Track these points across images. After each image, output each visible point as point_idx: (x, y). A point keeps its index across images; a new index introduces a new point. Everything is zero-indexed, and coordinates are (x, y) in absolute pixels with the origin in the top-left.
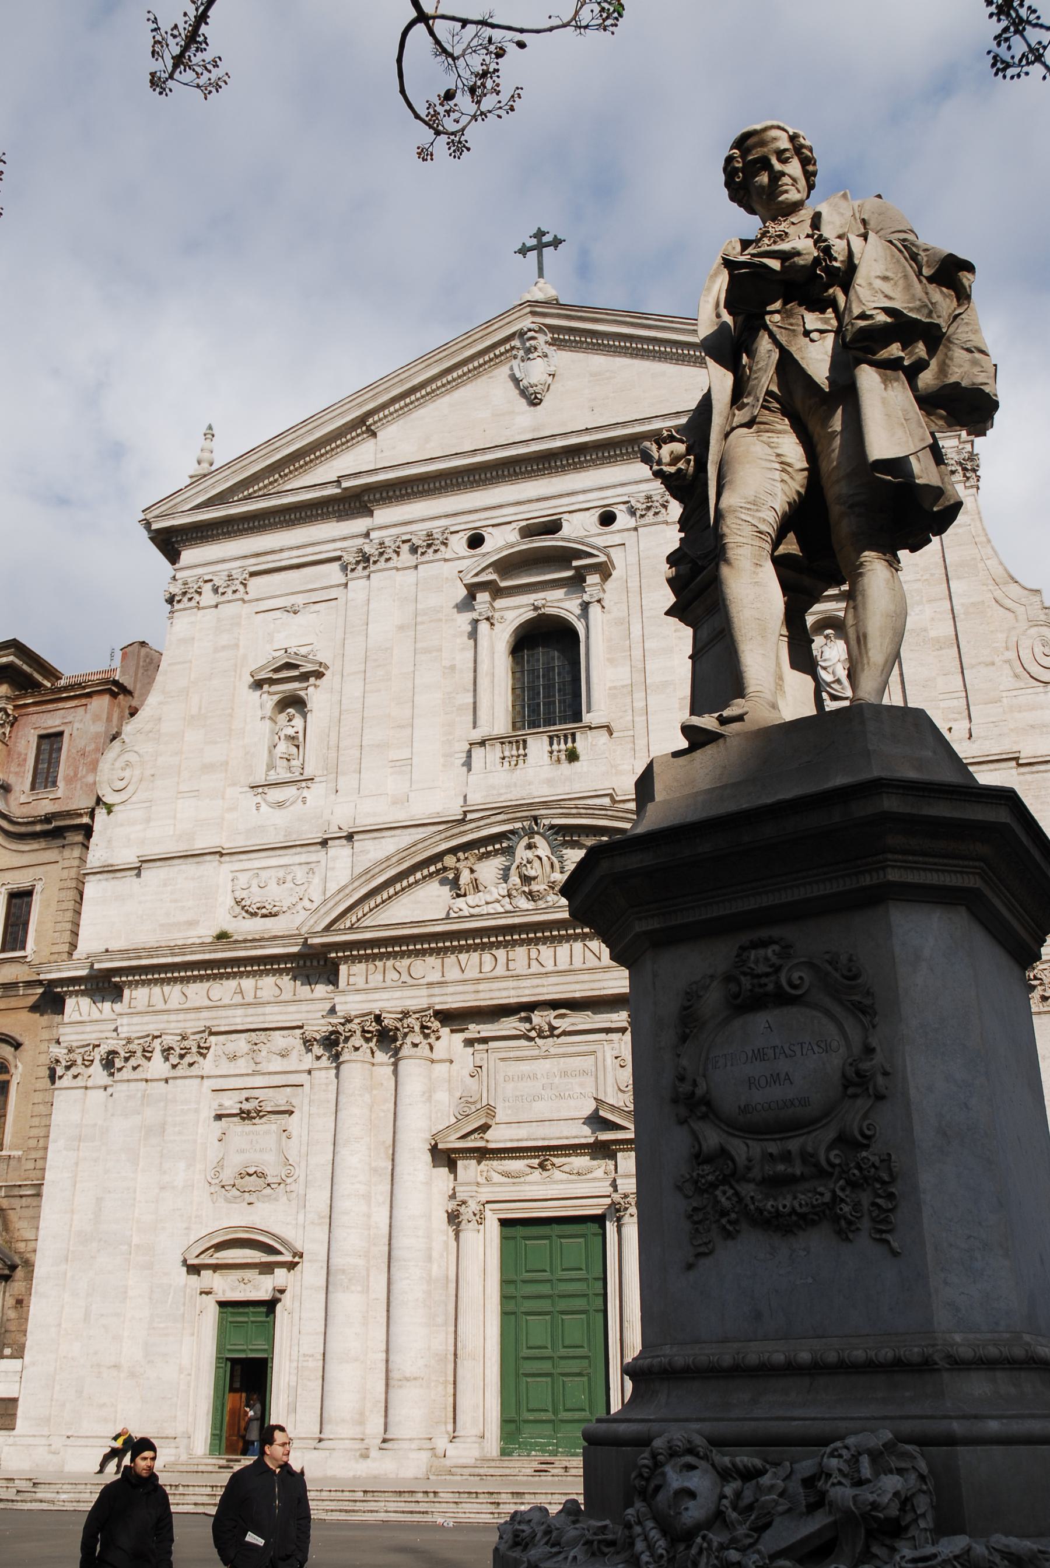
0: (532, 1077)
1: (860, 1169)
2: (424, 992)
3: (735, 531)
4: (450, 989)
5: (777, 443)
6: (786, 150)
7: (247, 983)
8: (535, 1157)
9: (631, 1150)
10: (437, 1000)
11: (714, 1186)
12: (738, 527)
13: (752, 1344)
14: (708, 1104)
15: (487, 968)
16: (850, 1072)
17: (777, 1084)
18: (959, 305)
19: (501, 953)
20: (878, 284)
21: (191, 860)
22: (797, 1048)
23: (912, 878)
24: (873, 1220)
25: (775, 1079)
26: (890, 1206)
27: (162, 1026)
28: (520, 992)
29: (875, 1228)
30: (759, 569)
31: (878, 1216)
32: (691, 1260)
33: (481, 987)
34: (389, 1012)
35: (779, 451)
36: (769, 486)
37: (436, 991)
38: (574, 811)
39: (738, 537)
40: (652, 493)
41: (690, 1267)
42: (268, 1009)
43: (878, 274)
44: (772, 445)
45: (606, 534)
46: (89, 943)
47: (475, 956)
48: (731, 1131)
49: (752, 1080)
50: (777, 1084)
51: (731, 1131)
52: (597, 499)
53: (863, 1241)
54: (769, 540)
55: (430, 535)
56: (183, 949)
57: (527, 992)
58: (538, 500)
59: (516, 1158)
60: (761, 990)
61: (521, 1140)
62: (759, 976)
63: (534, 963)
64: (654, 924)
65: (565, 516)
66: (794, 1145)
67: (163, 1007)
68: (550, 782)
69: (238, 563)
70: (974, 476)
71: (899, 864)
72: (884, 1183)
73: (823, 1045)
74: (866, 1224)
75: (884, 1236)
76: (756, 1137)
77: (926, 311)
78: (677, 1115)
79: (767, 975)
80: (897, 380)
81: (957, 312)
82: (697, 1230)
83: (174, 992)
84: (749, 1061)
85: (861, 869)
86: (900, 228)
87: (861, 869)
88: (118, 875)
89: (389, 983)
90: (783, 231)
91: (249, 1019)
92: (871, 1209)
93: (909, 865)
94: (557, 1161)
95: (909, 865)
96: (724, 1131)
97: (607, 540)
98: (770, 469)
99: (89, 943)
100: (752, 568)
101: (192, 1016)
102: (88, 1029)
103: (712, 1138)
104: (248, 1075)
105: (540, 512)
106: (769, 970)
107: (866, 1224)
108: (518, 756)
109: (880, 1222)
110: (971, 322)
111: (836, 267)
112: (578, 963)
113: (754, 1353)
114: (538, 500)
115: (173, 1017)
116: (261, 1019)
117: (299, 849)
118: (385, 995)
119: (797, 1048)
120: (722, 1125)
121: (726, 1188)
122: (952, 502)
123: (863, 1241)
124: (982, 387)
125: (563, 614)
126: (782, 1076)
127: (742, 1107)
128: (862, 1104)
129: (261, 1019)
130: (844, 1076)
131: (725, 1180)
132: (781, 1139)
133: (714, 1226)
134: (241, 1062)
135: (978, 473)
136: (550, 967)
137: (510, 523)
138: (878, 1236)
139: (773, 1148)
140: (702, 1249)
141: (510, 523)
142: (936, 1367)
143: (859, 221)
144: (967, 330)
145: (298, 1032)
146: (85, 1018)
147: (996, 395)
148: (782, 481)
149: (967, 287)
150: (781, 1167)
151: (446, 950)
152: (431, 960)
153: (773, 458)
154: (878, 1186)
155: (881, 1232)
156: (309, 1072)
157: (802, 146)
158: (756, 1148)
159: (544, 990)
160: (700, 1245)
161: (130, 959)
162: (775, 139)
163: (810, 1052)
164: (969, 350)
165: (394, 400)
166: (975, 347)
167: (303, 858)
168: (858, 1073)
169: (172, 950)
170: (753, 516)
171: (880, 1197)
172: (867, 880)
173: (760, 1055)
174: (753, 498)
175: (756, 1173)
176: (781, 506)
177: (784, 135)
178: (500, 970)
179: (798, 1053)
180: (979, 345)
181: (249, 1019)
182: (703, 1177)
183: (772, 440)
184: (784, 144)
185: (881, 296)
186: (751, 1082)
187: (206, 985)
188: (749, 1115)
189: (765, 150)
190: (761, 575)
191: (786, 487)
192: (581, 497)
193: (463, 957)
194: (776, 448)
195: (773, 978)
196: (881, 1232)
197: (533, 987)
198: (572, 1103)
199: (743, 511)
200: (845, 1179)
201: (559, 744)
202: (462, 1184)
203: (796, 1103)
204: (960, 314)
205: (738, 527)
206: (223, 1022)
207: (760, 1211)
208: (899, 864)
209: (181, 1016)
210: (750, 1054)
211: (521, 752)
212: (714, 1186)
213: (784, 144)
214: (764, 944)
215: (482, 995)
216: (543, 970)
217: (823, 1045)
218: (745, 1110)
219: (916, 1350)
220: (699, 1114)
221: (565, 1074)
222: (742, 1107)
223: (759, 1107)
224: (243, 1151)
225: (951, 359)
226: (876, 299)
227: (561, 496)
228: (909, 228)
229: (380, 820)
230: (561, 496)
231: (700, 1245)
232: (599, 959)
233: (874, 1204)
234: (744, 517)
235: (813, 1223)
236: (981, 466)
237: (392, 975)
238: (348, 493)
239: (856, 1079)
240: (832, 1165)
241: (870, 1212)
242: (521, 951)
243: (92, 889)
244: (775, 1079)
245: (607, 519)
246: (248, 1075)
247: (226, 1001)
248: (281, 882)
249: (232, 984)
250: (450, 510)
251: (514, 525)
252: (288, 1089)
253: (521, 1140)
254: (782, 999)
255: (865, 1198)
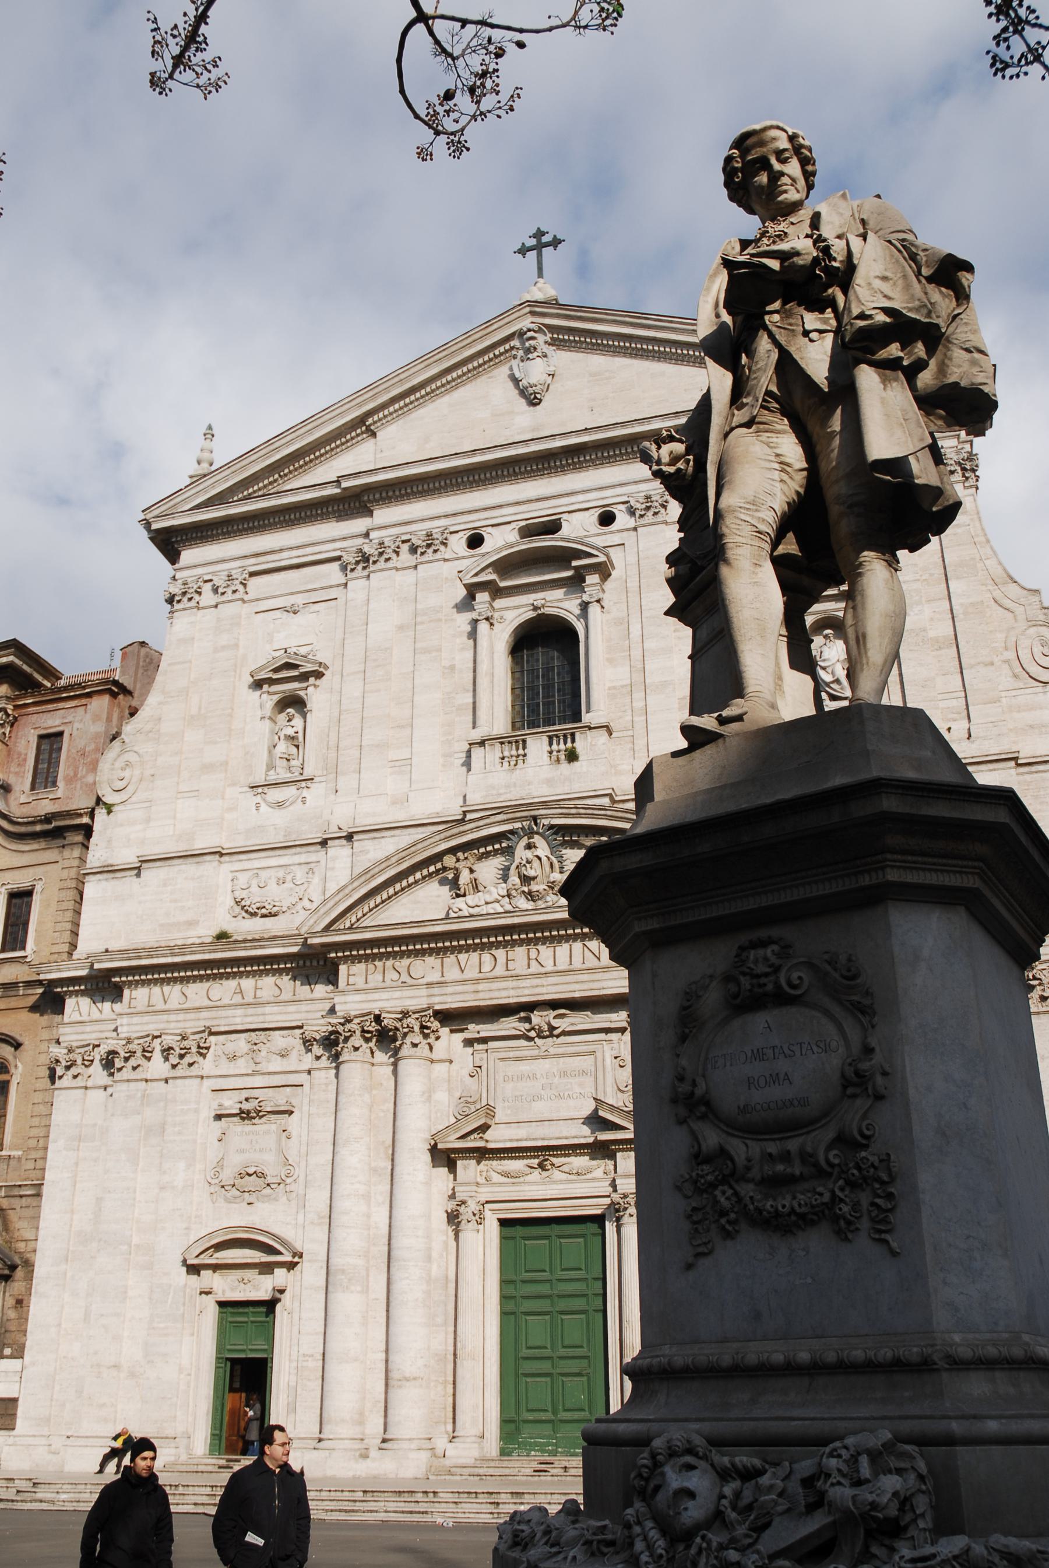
0: (532, 1077)
1: (859, 1169)
2: (424, 992)
3: (734, 531)
4: (450, 989)
5: (777, 443)
6: (785, 150)
7: (247, 983)
8: (535, 1157)
9: (630, 1150)
10: (436, 1000)
11: (713, 1186)
12: (738, 527)
13: (751, 1344)
14: (707, 1104)
15: (486, 968)
16: (850, 1072)
17: (777, 1084)
18: (958, 305)
19: (500, 953)
20: (878, 284)
21: (190, 860)
22: (796, 1048)
23: (911, 878)
24: (873, 1220)
25: (775, 1079)
26: (889, 1206)
27: (162, 1026)
28: (520, 992)
29: (874, 1228)
30: (758, 569)
31: (877, 1216)
32: (691, 1260)
33: (480, 987)
34: (389, 1012)
35: (778, 451)
36: (768, 486)
37: (436, 991)
38: (574, 811)
39: (737, 537)
40: (651, 493)
41: (689, 1267)
42: (268, 1009)
43: (878, 274)
44: (772, 445)
45: (605, 534)
46: (89, 943)
47: (474, 956)
48: (730, 1131)
49: (752, 1080)
50: (777, 1084)
51: (730, 1131)
52: (596, 499)
53: (863, 1241)
54: (768, 540)
55: (429, 535)
56: (183, 949)
57: (527, 992)
58: (538, 500)
59: (516, 1158)
60: (761, 990)
61: (521, 1140)
62: (758, 976)
63: (533, 963)
64: (653, 924)
65: (564, 516)
66: (793, 1145)
67: (163, 1007)
68: (549, 782)
69: (238, 563)
70: (973, 476)
71: (898, 864)
72: (883, 1183)
73: (822, 1045)
74: (865, 1224)
75: (883, 1236)
76: (755, 1137)
77: (925, 311)
78: (676, 1115)
79: (766, 975)
80: (896, 380)
81: (956, 312)
82: (696, 1230)
83: (174, 992)
84: (749, 1061)
85: (860, 869)
86: (899, 228)
87: (860, 869)
88: (118, 875)
89: (388, 983)
90: (783, 231)
91: (249, 1019)
92: (871, 1209)
93: (908, 865)
94: (556, 1161)
95: (908, 865)
96: (723, 1131)
97: (606, 540)
98: (770, 469)
99: (89, 943)
100: (752, 568)
101: (192, 1016)
102: (88, 1029)
103: (712, 1138)
104: (247, 1075)
105: (540, 512)
106: (768, 970)
107: (865, 1224)
108: (518, 756)
109: (879, 1222)
110: (971, 322)
111: (836, 267)
112: (577, 963)
113: (754, 1353)
114: (538, 500)
115: (173, 1017)
116: (261, 1019)
117: (298, 849)
118: (385, 995)
119: (796, 1048)
120: (722, 1125)
121: (726, 1188)
122: (951, 502)
123: (863, 1241)
124: (981, 387)
125: (563, 614)
126: (782, 1076)
127: (742, 1107)
128: (861, 1104)
129: (261, 1019)
130: (843, 1076)
131: (724, 1180)
132: (780, 1139)
133: (713, 1226)
134: (241, 1062)
135: (977, 473)
136: (549, 967)
137: (509, 523)
138: (877, 1236)
139: (772, 1148)
140: (701, 1249)
141: (509, 523)
142: (935, 1367)
143: (858, 221)
144: (966, 330)
145: (298, 1032)
146: (85, 1018)
147: (995, 395)
148: (782, 481)
149: (966, 287)
150: (780, 1167)
151: (445, 950)
152: (431, 960)
153: (773, 458)
154: (877, 1186)
155: (880, 1232)
156: (309, 1072)
157: (802, 146)
158: (756, 1148)
159: (544, 990)
160: (699, 1245)
161: (130, 959)
162: (774, 139)
163: (809, 1052)
164: (968, 350)
165: (393, 400)
166: (974, 347)
167: (303, 858)
168: (857, 1073)
169: (172, 950)
170: (753, 516)
171: (880, 1197)
172: (866, 880)
173: (759, 1055)
174: (752, 498)
175: (755, 1173)
176: (781, 506)
177: (784, 135)
178: (500, 970)
179: (798, 1053)
180: (978, 345)
181: (249, 1019)
182: (702, 1177)
183: (771, 440)
184: (784, 144)
185: (880, 296)
186: (750, 1082)
187: (206, 985)
188: (748, 1115)
189: (765, 150)
190: (760, 575)
191: (785, 487)
192: (581, 497)
193: (463, 957)
194: (775, 448)
195: (772, 978)
196: (880, 1232)
197: (533, 987)
198: (571, 1103)
199: (743, 511)
200: (844, 1179)
201: (558, 744)
202: (461, 1184)
203: (796, 1103)
204: (959, 314)
205: (738, 527)
206: (223, 1022)
207: (760, 1211)
208: (898, 864)
209: (181, 1016)
210: (749, 1054)
211: (521, 752)
212: (713, 1186)
213: (784, 144)
214: (763, 944)
215: (481, 995)
216: (543, 970)
217: (822, 1045)
218: (744, 1110)
219: (915, 1350)
220: (698, 1114)
221: (564, 1074)
222: (742, 1107)
223: (758, 1107)
224: (242, 1151)
225: (951, 359)
226: (875, 299)
227: (560, 496)
228: (908, 228)
229: (380, 820)
230: (560, 496)
231: (699, 1245)
232: (599, 959)
233: (873, 1204)
234: (743, 517)
235: (813, 1223)
236: (981, 466)
237: (391, 975)
238: (348, 493)
239: (855, 1079)
240: (831, 1165)
241: (869, 1212)
242: (520, 951)
243: (92, 889)
244: (775, 1079)
245: (607, 519)
246: (247, 1075)
247: (226, 1001)
248: (281, 882)
249: (232, 984)
250: (449, 510)
251: (513, 525)
252: (288, 1089)
253: (521, 1140)
254: (782, 999)
255: (865, 1198)
